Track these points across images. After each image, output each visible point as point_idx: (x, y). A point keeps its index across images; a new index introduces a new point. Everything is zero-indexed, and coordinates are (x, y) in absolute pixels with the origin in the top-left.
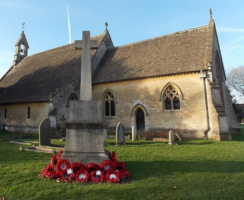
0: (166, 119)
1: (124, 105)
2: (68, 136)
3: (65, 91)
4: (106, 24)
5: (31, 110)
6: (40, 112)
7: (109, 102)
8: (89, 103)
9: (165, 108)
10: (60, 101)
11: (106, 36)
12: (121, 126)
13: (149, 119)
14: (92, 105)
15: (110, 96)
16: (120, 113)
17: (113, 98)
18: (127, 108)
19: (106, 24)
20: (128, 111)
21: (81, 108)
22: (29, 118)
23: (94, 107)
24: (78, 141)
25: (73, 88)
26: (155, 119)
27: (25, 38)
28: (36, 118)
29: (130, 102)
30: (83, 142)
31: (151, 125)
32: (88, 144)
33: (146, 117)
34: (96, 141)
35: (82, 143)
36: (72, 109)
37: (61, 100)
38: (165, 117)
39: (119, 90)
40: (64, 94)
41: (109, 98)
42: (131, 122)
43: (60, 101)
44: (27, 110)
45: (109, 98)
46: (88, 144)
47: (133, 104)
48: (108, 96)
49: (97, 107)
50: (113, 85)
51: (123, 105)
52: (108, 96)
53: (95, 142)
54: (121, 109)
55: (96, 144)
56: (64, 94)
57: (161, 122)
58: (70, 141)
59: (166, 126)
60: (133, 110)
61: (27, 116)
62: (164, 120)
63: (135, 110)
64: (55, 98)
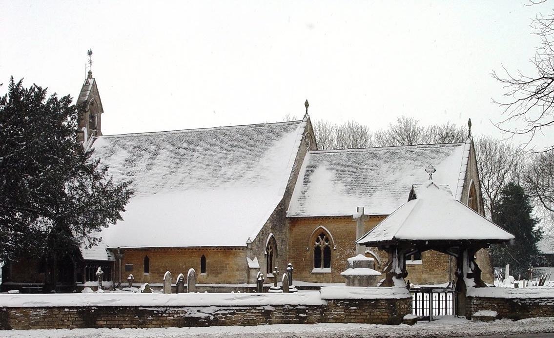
19: (307, 105)
25: (270, 227)
28: (221, 273)
41: (322, 241)
45: (322, 241)
51: (344, 254)
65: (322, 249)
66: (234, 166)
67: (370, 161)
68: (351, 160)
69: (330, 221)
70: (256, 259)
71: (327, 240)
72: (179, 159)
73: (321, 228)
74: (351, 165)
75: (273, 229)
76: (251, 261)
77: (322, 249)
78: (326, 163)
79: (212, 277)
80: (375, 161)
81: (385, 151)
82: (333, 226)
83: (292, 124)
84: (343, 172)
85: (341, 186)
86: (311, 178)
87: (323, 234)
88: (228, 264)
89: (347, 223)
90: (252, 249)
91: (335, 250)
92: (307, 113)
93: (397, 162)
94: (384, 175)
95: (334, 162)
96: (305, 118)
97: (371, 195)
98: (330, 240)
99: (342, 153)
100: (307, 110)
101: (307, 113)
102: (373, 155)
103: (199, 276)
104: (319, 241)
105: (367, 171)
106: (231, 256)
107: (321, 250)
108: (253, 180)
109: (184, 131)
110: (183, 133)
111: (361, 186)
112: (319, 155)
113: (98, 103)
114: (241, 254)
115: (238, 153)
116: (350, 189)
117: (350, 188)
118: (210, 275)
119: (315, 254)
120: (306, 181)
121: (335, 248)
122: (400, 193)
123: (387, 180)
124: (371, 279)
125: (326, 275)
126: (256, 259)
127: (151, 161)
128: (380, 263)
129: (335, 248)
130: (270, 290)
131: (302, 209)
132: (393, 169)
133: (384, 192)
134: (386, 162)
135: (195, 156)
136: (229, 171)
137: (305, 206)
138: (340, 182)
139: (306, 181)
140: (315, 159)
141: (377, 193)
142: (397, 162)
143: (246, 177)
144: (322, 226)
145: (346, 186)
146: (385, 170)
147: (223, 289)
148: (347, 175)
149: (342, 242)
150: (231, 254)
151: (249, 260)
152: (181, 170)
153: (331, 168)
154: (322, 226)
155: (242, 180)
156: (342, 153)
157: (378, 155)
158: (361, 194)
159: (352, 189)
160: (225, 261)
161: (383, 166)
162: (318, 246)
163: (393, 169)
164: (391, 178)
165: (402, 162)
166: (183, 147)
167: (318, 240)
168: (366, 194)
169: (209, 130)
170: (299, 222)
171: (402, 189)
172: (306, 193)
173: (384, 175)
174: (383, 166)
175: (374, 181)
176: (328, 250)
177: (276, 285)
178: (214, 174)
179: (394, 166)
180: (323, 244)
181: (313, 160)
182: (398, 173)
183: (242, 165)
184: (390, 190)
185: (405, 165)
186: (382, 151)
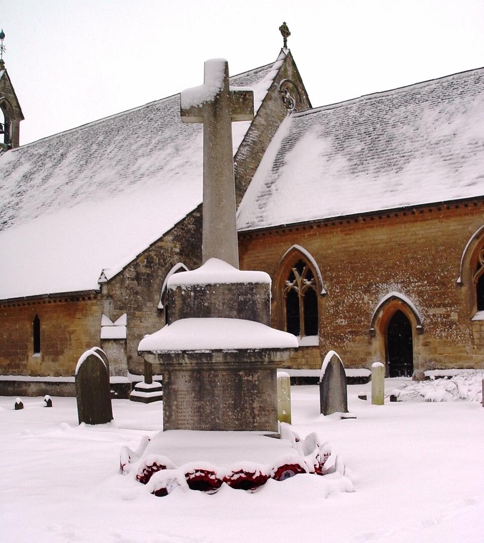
0: (476, 341)
1: (348, 300)
2: (169, 392)
3: (152, 258)
4: (285, 31)
5: (44, 327)
6: (74, 332)
7: (300, 294)
8: (230, 290)
9: (475, 308)
10: (137, 293)
11: (286, 70)
12: (336, 368)
13: (426, 344)
14: (241, 298)
15: (300, 273)
16: (336, 328)
17: (309, 280)
18: (357, 310)
19: (285, 31)
20: (360, 322)
21: (208, 307)
22: (37, 350)
23: (245, 302)
24: (199, 407)
25: (177, 250)
26: (445, 343)
27: (8, 84)
28: (62, 352)
29: (367, 291)
30: (215, 408)
31: (430, 361)
32: (230, 414)
33: (418, 339)
34: (256, 405)
35: (211, 412)
36: (177, 312)
37: (139, 289)
38: (476, 335)
39: (329, 251)
40: (148, 271)
41: (299, 279)
42: (369, 354)
43: (137, 293)
44: (29, 326)
45: (299, 279)
46: (230, 414)
47: (376, 298)
48: (296, 273)
49: (254, 302)
50: (309, 236)
51: (344, 302)
52: (296, 273)
53: (252, 409)
54: (336, 315)
55: (256, 412)
56: (148, 271)
57: (462, 352)
58: (174, 408)
59: (476, 363)
60: (376, 315)
61: (31, 345)
62: (473, 343)
63: (381, 314)
64: (118, 285)
65: (300, 294)
66: (156, 154)
67: (403, 109)
68: (366, 114)
69: (312, 232)
70: (123, 320)
71: (310, 275)
72: (87, 158)
73: (295, 249)
74: (365, 122)
75: (187, 255)
76: (111, 323)
77: (300, 294)
78: (319, 128)
79: (49, 363)
80: (411, 107)
81: (433, 86)
82: (318, 243)
83: (260, 71)
84: (349, 137)
85: (341, 162)
86: (288, 156)
87: (301, 263)
88: (74, 332)
89: (346, 235)
90: (109, 296)
91: (324, 295)
92: (285, 46)
93: (458, 100)
94: (429, 127)
95: (333, 123)
96: (282, 54)
97: (401, 169)
98: (315, 276)
99: (349, 106)
100: (285, 41)
101: (285, 46)
102: (408, 97)
103: (30, 359)
104: (294, 278)
105: (394, 126)
106: (78, 315)
107: (298, 298)
108: (178, 170)
109: (104, 120)
110: (104, 121)
111: (381, 156)
112: (307, 118)
113: (14, 104)
114: (95, 308)
115: (167, 133)
116: (357, 165)
117: (358, 163)
118: (45, 357)
119: (287, 306)
120: (278, 164)
121: (324, 292)
122: (463, 157)
123: (436, 135)
124: (252, 370)
125: (309, 351)
126: (123, 320)
127: (51, 170)
128: (422, 320)
129: (324, 292)
130: (134, 393)
131: (259, 215)
132: (448, 115)
133: (428, 159)
134: (435, 104)
135: (108, 151)
136: (145, 163)
137: (267, 208)
138: (339, 156)
139: (278, 164)
140: (300, 125)
141: (412, 167)
142: (458, 100)
143: (167, 168)
144: (297, 246)
145: (350, 160)
146: (431, 120)
147: (58, 388)
148: (355, 141)
149: (337, 277)
150: (76, 310)
151: (105, 320)
152: (82, 176)
153: (327, 134)
154: (297, 246)
155: (162, 173)
156: (349, 106)
157: (418, 96)
158: (378, 170)
159: (362, 164)
160: (68, 327)
161: (427, 112)
162: (293, 290)
163: (448, 115)
164: (445, 130)
165: (467, 98)
166: (97, 142)
167: (292, 278)
168: (390, 168)
169: (138, 109)
170: (254, 242)
171: (469, 146)
172: (273, 185)
173: (429, 127)
174: (427, 112)
175: (408, 143)
176: (311, 296)
177: (148, 381)
178: (123, 176)
179: (451, 108)
180: (300, 284)
181: (297, 126)
182: (458, 121)
183: (170, 149)
184: (441, 153)
185: (475, 103)
186: (426, 89)
